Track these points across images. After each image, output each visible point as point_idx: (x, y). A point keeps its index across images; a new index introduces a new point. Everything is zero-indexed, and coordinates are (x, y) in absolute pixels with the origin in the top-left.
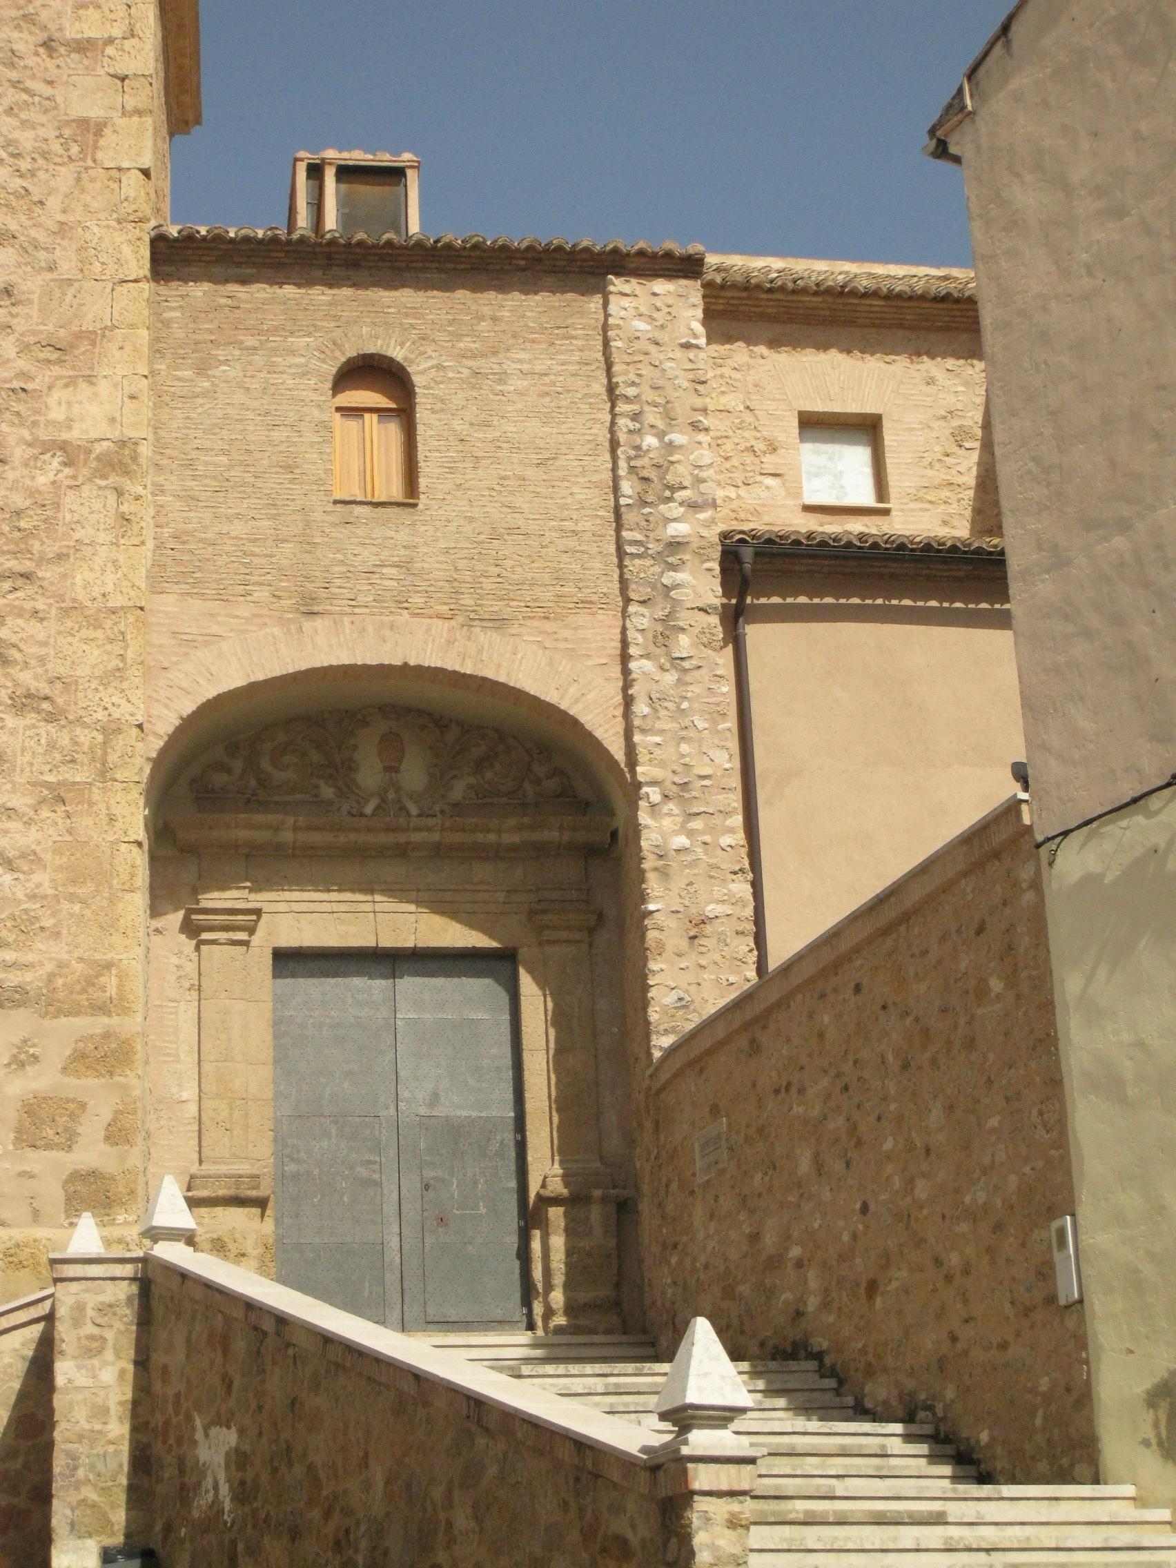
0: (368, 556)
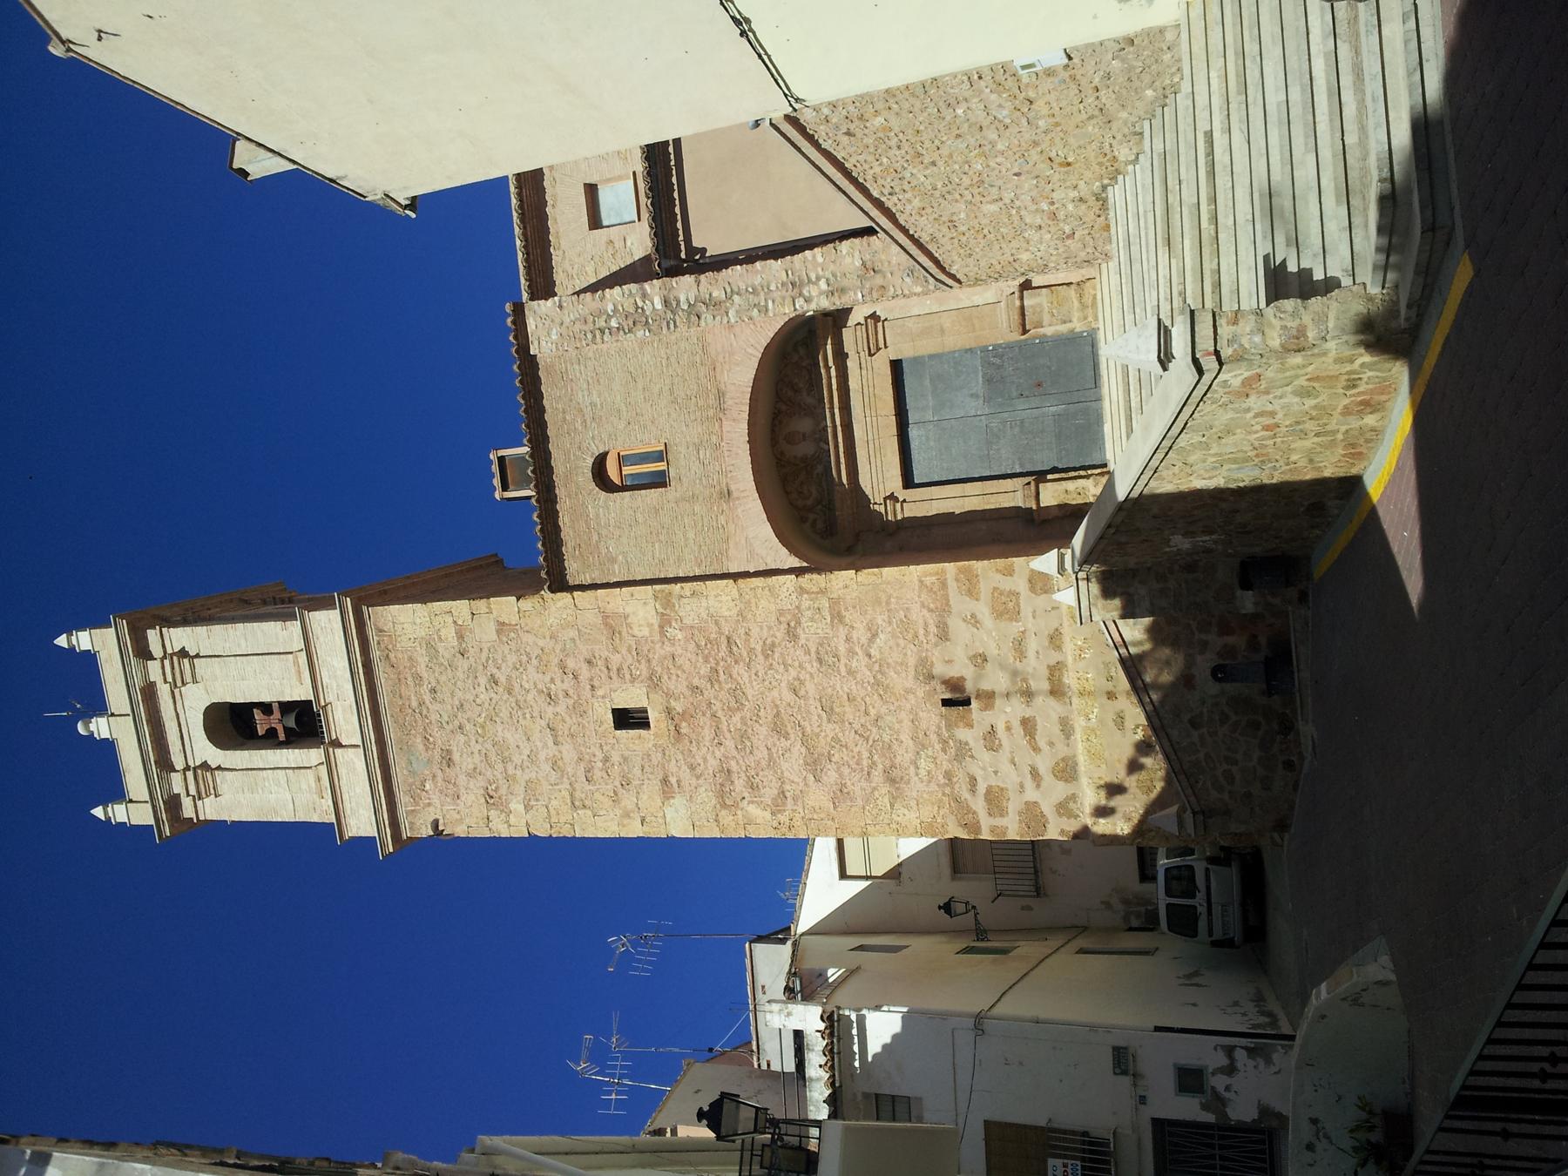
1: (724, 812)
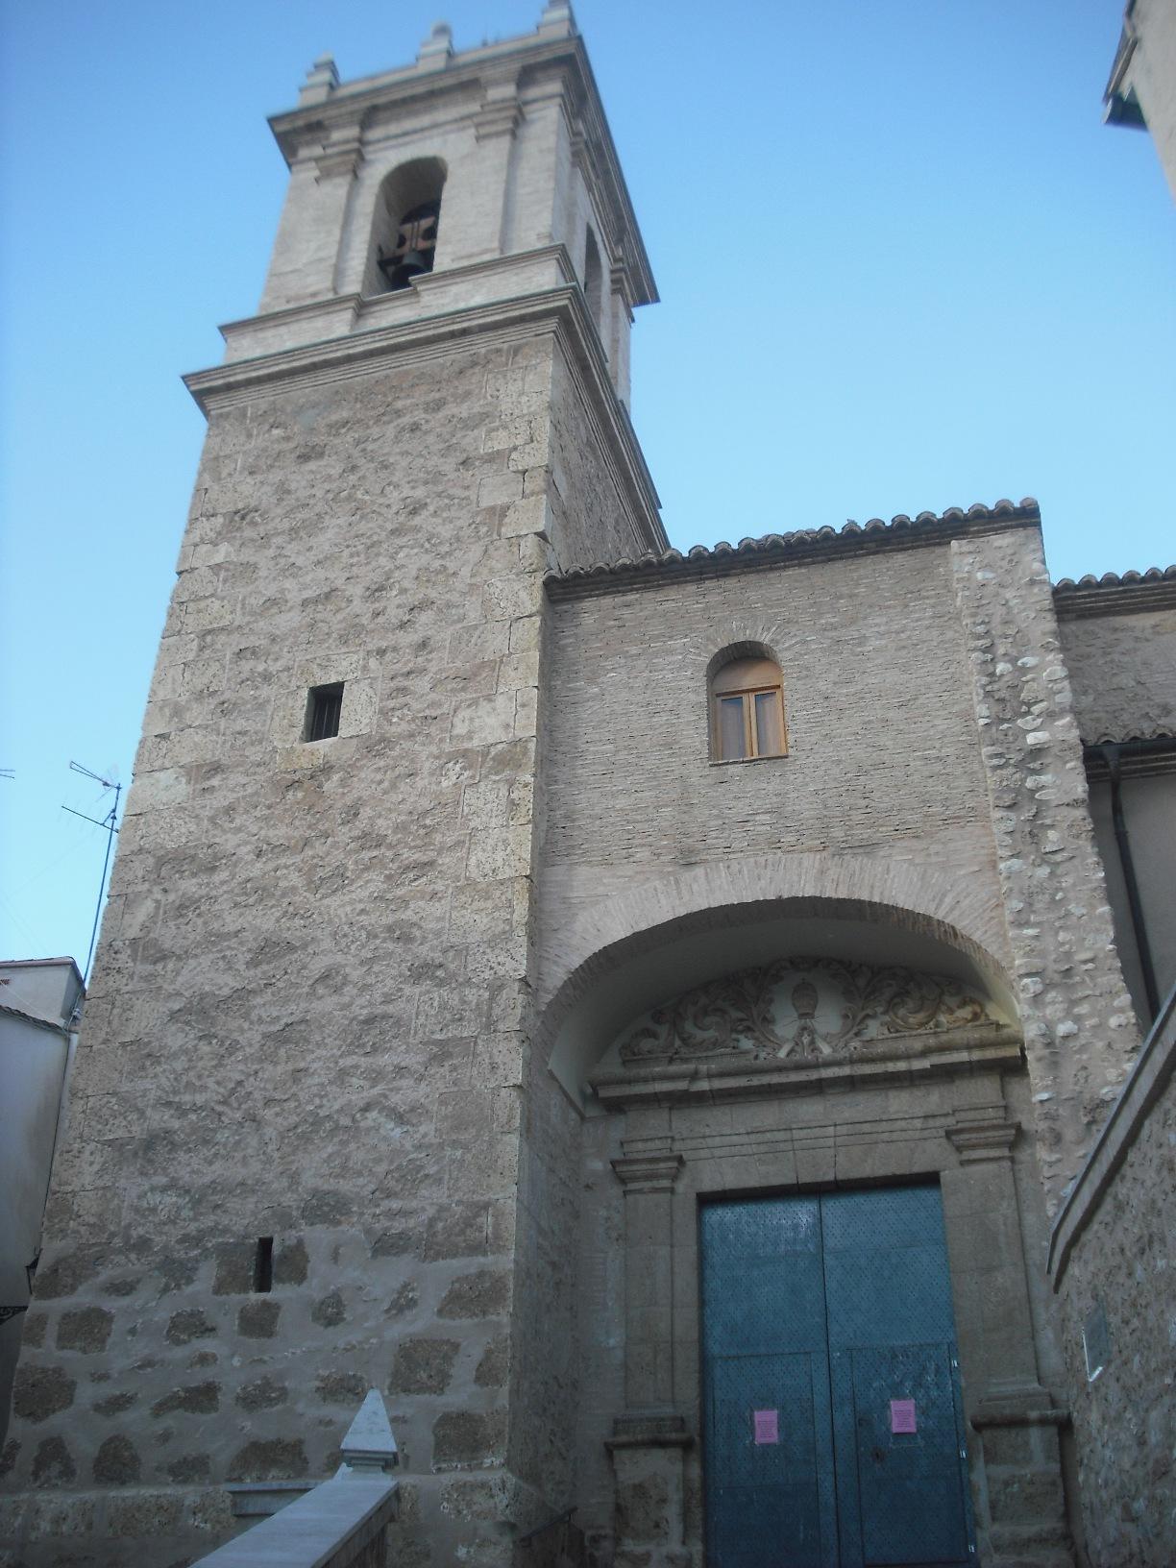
0: (741, 809)
1: (151, 861)
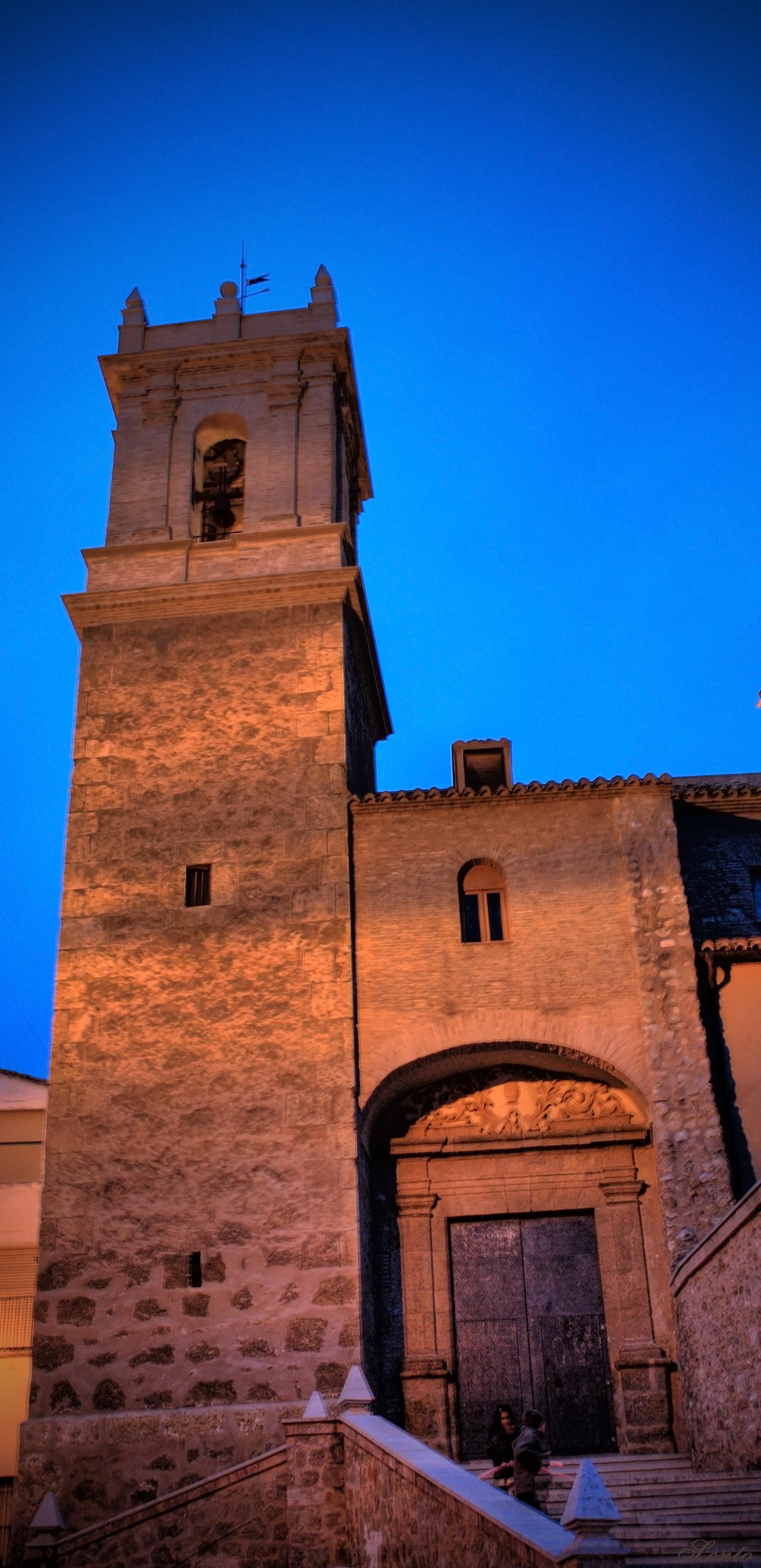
0: (482, 976)
1: (83, 986)
